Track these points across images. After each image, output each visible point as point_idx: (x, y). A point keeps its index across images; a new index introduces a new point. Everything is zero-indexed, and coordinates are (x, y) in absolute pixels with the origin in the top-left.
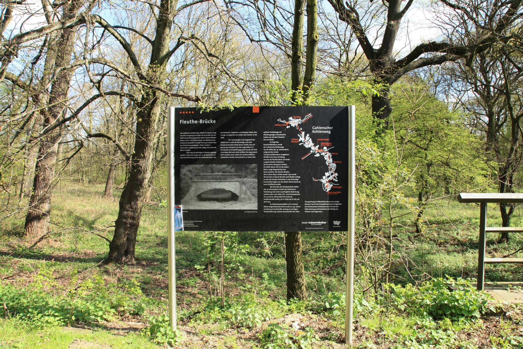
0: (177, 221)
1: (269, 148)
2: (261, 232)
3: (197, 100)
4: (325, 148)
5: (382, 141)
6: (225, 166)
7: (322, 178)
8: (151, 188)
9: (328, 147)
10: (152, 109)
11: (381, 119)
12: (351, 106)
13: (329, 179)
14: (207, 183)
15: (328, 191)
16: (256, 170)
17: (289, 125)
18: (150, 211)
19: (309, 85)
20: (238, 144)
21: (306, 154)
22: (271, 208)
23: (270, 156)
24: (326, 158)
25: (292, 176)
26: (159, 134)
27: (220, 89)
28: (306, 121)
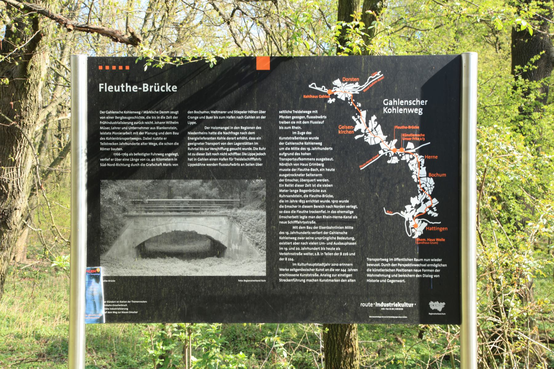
0: (91, 301)
1: (290, 146)
2: (268, 325)
3: (134, 41)
4: (410, 145)
5: (533, 128)
6: (196, 182)
7: (404, 209)
8: (27, 230)
9: (416, 144)
10: (30, 57)
11: (531, 80)
12: (468, 55)
13: (419, 210)
14: (159, 219)
15: (416, 236)
16: (263, 192)
17: (333, 96)
18: (23, 281)
19: (377, 10)
20: (226, 136)
21: (370, 157)
22: (294, 272)
23: (293, 162)
24: (413, 165)
25: (339, 204)
26: (47, 113)
27: (180, 17)
28: (370, 89)
